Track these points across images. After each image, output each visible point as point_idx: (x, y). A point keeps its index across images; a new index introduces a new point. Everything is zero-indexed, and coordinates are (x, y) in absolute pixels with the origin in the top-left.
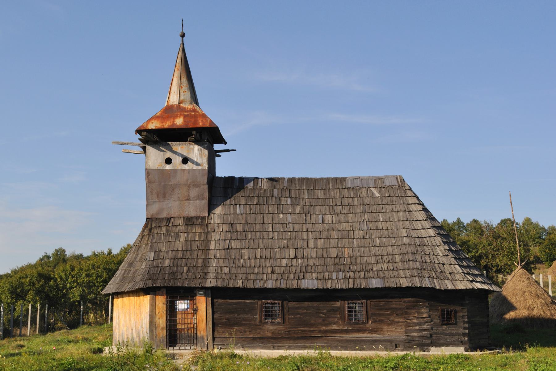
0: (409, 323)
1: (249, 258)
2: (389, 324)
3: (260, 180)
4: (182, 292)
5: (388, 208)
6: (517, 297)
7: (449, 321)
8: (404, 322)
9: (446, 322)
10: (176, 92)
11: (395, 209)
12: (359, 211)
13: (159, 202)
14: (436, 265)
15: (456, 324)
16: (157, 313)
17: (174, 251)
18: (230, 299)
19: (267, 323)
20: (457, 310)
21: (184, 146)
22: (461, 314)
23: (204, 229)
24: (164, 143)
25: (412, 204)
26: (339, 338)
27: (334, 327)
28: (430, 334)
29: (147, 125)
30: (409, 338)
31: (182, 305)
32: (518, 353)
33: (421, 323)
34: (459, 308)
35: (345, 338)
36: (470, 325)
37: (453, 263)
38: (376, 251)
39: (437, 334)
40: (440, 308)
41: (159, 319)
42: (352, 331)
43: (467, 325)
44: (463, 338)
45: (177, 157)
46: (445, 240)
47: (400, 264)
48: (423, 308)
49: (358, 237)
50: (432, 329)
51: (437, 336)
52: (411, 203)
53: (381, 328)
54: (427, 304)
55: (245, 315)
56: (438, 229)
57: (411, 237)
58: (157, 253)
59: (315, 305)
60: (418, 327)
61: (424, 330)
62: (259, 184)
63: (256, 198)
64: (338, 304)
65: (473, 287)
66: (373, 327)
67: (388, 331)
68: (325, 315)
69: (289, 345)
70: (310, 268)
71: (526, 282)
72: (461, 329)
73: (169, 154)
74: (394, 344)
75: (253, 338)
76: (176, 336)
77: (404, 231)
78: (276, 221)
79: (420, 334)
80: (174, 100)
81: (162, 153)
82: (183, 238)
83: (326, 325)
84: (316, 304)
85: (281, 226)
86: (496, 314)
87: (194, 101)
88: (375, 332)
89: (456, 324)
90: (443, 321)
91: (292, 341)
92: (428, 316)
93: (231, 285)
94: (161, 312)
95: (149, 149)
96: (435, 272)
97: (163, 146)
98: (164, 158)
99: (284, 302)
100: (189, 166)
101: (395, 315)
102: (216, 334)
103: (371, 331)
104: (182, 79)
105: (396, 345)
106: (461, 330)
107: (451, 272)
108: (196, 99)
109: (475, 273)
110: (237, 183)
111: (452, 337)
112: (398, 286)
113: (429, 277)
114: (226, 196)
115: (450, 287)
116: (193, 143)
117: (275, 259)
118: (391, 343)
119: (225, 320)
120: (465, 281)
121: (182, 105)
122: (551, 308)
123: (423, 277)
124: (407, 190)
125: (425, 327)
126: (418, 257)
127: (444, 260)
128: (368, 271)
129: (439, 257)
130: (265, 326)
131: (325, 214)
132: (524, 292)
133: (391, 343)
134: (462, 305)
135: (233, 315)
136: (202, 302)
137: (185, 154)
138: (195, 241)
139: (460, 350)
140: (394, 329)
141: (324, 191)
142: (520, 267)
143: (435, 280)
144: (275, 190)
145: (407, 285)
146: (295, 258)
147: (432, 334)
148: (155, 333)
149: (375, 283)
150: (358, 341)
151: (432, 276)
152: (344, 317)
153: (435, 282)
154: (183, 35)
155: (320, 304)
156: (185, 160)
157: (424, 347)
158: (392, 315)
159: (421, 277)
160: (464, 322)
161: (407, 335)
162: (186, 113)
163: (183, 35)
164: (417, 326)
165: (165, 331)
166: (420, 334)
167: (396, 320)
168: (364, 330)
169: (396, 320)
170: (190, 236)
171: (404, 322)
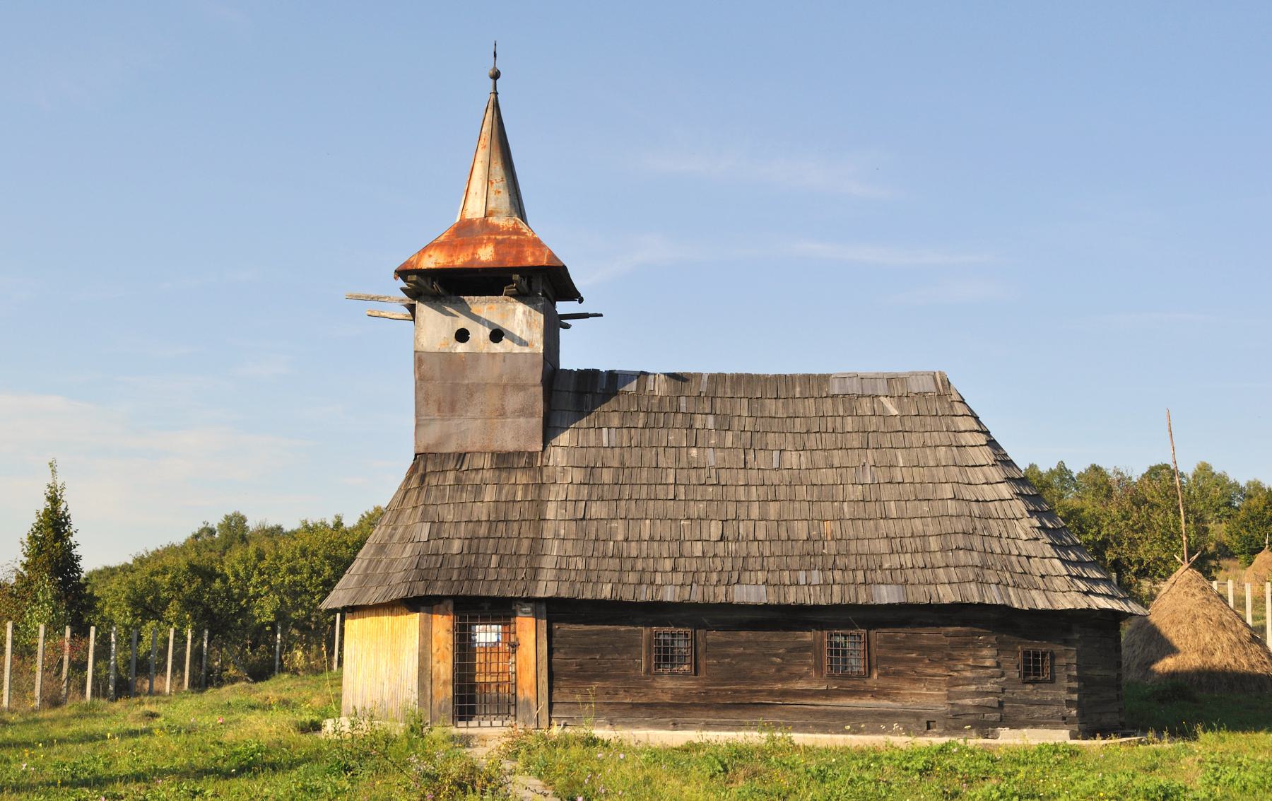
0: (956, 679)
1: (626, 540)
2: (914, 679)
3: (651, 377)
4: (486, 608)
5: (915, 439)
6: (1180, 627)
8: (946, 676)
11: (929, 441)
12: (856, 444)
13: (442, 420)
14: (1014, 559)
15: (1053, 681)
17: (471, 521)
18: (586, 624)
19: (663, 674)
20: (1055, 652)
21: (495, 306)
22: (1064, 661)
24: (454, 298)
25: (965, 431)
26: (809, 707)
27: (800, 685)
29: (419, 260)
30: (956, 709)
31: (486, 635)
33: (980, 678)
34: (1057, 648)
39: (1012, 702)
40: (1019, 647)
41: (438, 662)
43: (1075, 685)
44: (1066, 711)
45: (481, 326)
46: (1031, 508)
50: (1003, 690)
54: (993, 639)
55: (616, 656)
57: (963, 499)
59: (762, 639)
60: (973, 688)
61: (987, 693)
62: (650, 386)
63: (642, 414)
64: (809, 636)
65: (1089, 606)
68: (782, 659)
69: (707, 720)
70: (751, 560)
71: (1200, 596)
72: (1063, 691)
73: (463, 322)
74: (924, 721)
76: (472, 699)
78: (684, 463)
79: (978, 701)
80: (475, 209)
83: (783, 680)
84: (762, 636)
86: (1137, 661)
87: (516, 212)
88: (885, 695)
89: (1053, 681)
90: (1026, 675)
91: (712, 713)
92: (995, 664)
94: (442, 648)
96: (1010, 572)
97: (451, 304)
100: (505, 346)
101: (927, 661)
103: (875, 694)
104: (493, 165)
105: (928, 723)
106: (1063, 695)
107: (1044, 573)
109: (1095, 577)
111: (1044, 709)
113: (997, 584)
115: (1042, 604)
116: (513, 300)
119: (574, 667)
120: (1073, 593)
121: (491, 220)
122: (1249, 651)
123: (987, 583)
125: (989, 686)
126: (977, 542)
127: (1030, 548)
128: (872, 570)
129: (1019, 542)
130: (658, 680)
131: (784, 450)
132: (1195, 618)
133: (918, 720)
134: (1066, 642)
135: (593, 657)
136: (527, 629)
137: (497, 321)
139: (1061, 736)
141: (783, 403)
144: (683, 399)
146: (721, 540)
147: (1003, 702)
149: (887, 595)
150: (849, 713)
151: (1005, 582)
152: (822, 664)
153: (1011, 593)
154: (496, 76)
157: (985, 728)
158: (921, 660)
159: (981, 582)
160: (1070, 678)
162: (499, 237)
163: (496, 76)
164: (971, 684)
166: (978, 701)
167: (929, 671)
168: (864, 691)
169: (929, 671)
170: (504, 492)
171: (946, 676)
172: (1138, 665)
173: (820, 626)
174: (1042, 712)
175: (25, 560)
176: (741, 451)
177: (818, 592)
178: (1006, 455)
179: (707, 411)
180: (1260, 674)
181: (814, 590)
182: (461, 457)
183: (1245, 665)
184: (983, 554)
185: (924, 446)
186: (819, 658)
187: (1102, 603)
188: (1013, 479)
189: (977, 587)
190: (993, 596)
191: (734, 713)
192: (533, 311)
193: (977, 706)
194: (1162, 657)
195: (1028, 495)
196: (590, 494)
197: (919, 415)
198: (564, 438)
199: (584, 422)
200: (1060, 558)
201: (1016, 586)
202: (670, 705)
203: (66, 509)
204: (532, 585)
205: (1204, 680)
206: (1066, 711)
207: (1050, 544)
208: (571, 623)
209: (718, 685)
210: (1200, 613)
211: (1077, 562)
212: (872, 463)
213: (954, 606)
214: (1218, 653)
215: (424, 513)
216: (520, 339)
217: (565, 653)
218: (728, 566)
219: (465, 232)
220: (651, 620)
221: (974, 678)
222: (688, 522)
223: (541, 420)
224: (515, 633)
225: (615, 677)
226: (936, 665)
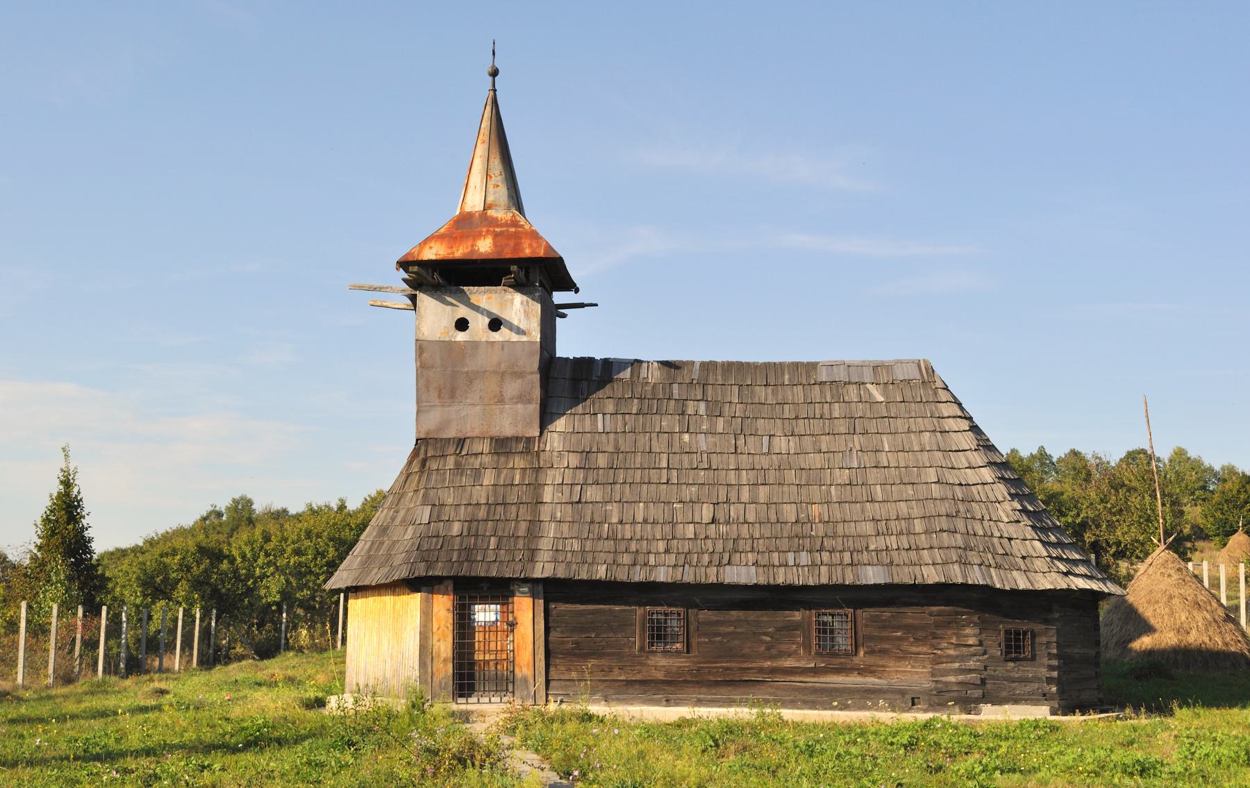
0: (940, 656)
1: (621, 522)
2: (899, 657)
3: (645, 365)
4: (485, 588)
5: (900, 425)
6: (1156, 606)
8: (930, 654)
9: (1013, 655)
11: (914, 427)
12: (843, 429)
13: (442, 406)
14: (996, 540)
15: (1033, 658)
16: (435, 629)
17: (470, 504)
21: (494, 296)
22: (1044, 639)
24: (453, 288)
25: (949, 417)
27: (789, 663)
29: (420, 252)
30: (940, 686)
31: (485, 614)
33: (963, 656)
34: (1038, 627)
35: (810, 684)
37: (1030, 537)
38: (874, 510)
39: (994, 680)
40: (1001, 626)
41: (439, 641)
43: (1055, 663)
44: (1046, 687)
46: (1013, 491)
48: (968, 625)
49: (839, 481)
50: (986, 668)
51: (994, 684)
53: (883, 666)
54: (975, 618)
55: (611, 635)
57: (947, 483)
60: (957, 665)
61: (970, 671)
62: (643, 373)
63: (636, 401)
64: (797, 616)
65: (1069, 586)
66: (867, 663)
67: (896, 671)
69: (699, 696)
70: (742, 542)
71: (1176, 577)
72: (1043, 669)
73: (463, 311)
74: (909, 697)
76: (471, 676)
78: (676, 448)
79: (961, 678)
80: (474, 202)
81: (449, 308)
82: (488, 478)
84: (752, 615)
86: (1115, 640)
87: (514, 204)
88: (871, 672)
90: (1007, 653)
91: (704, 690)
92: (977, 643)
93: (584, 576)
96: (992, 554)
97: (451, 294)
99: (690, 611)
100: (503, 335)
102: (553, 674)
103: (862, 672)
104: (491, 160)
105: (913, 699)
106: (1044, 672)
107: (1025, 554)
109: (1074, 558)
111: (1025, 686)
113: (980, 565)
115: (1023, 584)
119: (570, 646)
122: (1223, 630)
123: (970, 564)
124: (939, 390)
125: (971, 664)
126: (960, 525)
127: (1011, 530)
131: (774, 435)
132: (1171, 598)
133: (903, 697)
135: (588, 635)
136: (525, 608)
137: (495, 310)
139: (1041, 712)
143: (992, 570)
144: (675, 386)
145: (937, 580)
147: (985, 679)
148: (430, 670)
149: (873, 576)
150: (836, 690)
151: (987, 563)
152: (810, 642)
153: (993, 574)
154: (494, 73)
156: (495, 324)
158: (906, 639)
159: (964, 563)
160: (1050, 656)
162: (498, 230)
163: (494, 73)
164: (955, 662)
165: (450, 666)
166: (961, 678)
167: (914, 649)
169: (914, 649)
171: (930, 654)
172: (1116, 644)
173: (808, 606)
175: (39, 541)
177: (807, 573)
178: (988, 440)
180: (1234, 652)
184: (966, 536)
187: (1081, 584)
188: (995, 464)
190: (976, 577)
191: (724, 690)
192: (530, 300)
194: (1139, 636)
195: (1010, 479)
197: (904, 402)
198: (560, 424)
199: (579, 409)
203: (79, 492)
204: (529, 566)
205: (1180, 658)
206: (1046, 687)
207: (1031, 526)
208: (567, 603)
209: (709, 662)
211: (1057, 543)
212: (858, 448)
213: (938, 587)
214: (1194, 632)
216: (518, 328)
217: (562, 632)
218: (719, 547)
219: (465, 225)
220: (644, 600)
221: (957, 656)
224: (513, 612)
225: (610, 654)
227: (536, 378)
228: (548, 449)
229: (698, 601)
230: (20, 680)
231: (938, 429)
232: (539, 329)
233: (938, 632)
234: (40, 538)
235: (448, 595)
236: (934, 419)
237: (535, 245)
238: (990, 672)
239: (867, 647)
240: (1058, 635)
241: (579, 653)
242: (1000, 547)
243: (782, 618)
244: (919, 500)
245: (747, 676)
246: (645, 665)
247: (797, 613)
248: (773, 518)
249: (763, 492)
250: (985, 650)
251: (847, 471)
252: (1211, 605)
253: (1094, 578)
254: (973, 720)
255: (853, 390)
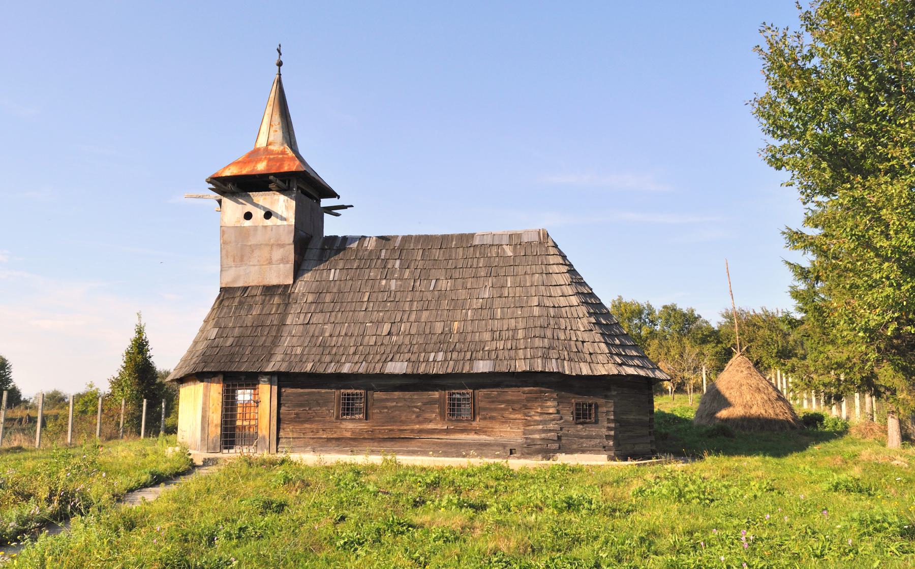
0: (529, 421)
1: (331, 336)
2: (503, 422)
3: (368, 239)
4: (243, 379)
5: (521, 270)
6: (732, 391)
7: (587, 418)
8: (523, 419)
9: (581, 420)
10: (265, 132)
11: (529, 271)
12: (483, 274)
13: (236, 267)
14: (573, 343)
15: (596, 422)
16: (211, 406)
17: (242, 327)
18: (302, 388)
19: (346, 419)
20: (598, 403)
21: (267, 197)
22: (605, 409)
23: (284, 300)
24: (244, 194)
25: (553, 264)
26: (436, 440)
27: (431, 426)
28: (558, 436)
29: (223, 172)
30: (529, 441)
31: (243, 395)
32: (432, 478)
33: (545, 421)
34: (601, 401)
36: (618, 424)
37: (597, 341)
38: (494, 325)
39: (568, 437)
40: (573, 400)
41: (213, 413)
42: (454, 431)
43: (613, 425)
44: (605, 442)
45: (258, 210)
46: (592, 311)
47: (522, 341)
48: (549, 400)
49: (475, 307)
50: (561, 429)
51: (568, 439)
52: (552, 263)
53: (492, 428)
54: (555, 395)
55: (319, 408)
56: (586, 297)
57: (544, 306)
58: (221, 329)
59: (407, 397)
60: (540, 427)
61: (550, 431)
62: (365, 244)
63: (357, 260)
64: (436, 395)
65: (619, 372)
66: (481, 426)
67: (500, 431)
68: (420, 409)
69: (372, 448)
70: (403, 346)
71: (745, 372)
72: (603, 429)
73: (249, 208)
74: (508, 449)
75: (327, 438)
76: (233, 436)
77: (536, 299)
78: (376, 289)
79: (543, 435)
80: (262, 143)
81: (240, 206)
82: (256, 311)
83: (420, 423)
84: (408, 395)
85: (380, 295)
86: (706, 412)
87: (287, 142)
88: (483, 432)
89: (596, 422)
90: (577, 418)
91: (376, 444)
92: (555, 412)
93: (297, 370)
94: (215, 404)
95: (225, 200)
96: (568, 351)
97: (242, 197)
98: (243, 212)
99: (368, 392)
100: (273, 221)
101: (511, 410)
102: (282, 434)
103: (477, 432)
104: (274, 115)
105: (511, 450)
106: (604, 432)
107: (591, 352)
108: (292, 141)
109: (632, 354)
110: (338, 244)
111: (590, 441)
112: (512, 370)
113: (557, 359)
114: (322, 258)
115: (585, 371)
116: (278, 193)
117: (363, 336)
118: (504, 448)
119: (293, 416)
120: (610, 365)
121: (270, 147)
122: (775, 406)
123: (549, 358)
124: (550, 248)
125: (551, 426)
126: (549, 333)
127: (586, 336)
128: (477, 350)
129: (578, 333)
130: (344, 423)
131: (439, 279)
132: (741, 385)
133: (504, 448)
134: (606, 397)
136: (266, 392)
137: (269, 207)
138: (270, 314)
139: (600, 460)
140: (509, 429)
141: (444, 252)
142: (739, 354)
143: (566, 362)
144: (384, 251)
145: (524, 369)
146: (388, 334)
147: (561, 436)
148: (207, 432)
149: (483, 367)
150: (460, 444)
151: (563, 358)
152: (444, 412)
153: (566, 365)
154: (280, 64)
155: (415, 395)
156: (268, 215)
157: (547, 453)
158: (507, 409)
159: (546, 358)
160: (609, 421)
161: (526, 436)
162: (272, 157)
163: (280, 64)
164: (539, 425)
165: (219, 429)
166: (543, 435)
167: (512, 416)
168: (470, 430)
169: (512, 416)
170: (265, 309)
171: (523, 419)
172: (707, 415)
173: (443, 388)
174: (589, 443)
175: (124, 365)
176: (413, 281)
177: (439, 366)
178: (582, 279)
179: (396, 258)
180: (782, 420)
181: (438, 365)
182: (245, 289)
183: (772, 414)
184: (551, 341)
185: (525, 274)
186: (442, 408)
187: (631, 371)
188: (583, 293)
189: (542, 361)
190: (553, 366)
191: (389, 444)
192: (289, 199)
193: (543, 439)
194: (720, 410)
195: (592, 304)
196: (315, 309)
197: (525, 255)
198: (308, 276)
199: (322, 267)
200: (606, 343)
201: (570, 360)
202: (351, 439)
203: (146, 337)
204: (265, 364)
205: (745, 423)
206: (605, 442)
207: (601, 333)
208: (293, 388)
209: (379, 426)
210: (745, 383)
211: (620, 345)
212: (491, 285)
213: (524, 373)
214: (755, 407)
215: (217, 322)
216: (281, 216)
217: (288, 407)
218: (388, 351)
219: (254, 155)
220: (340, 386)
221: (541, 421)
222: (371, 324)
223: (293, 265)
224: (258, 394)
226: (517, 412)
227: (291, 249)
228: (296, 291)
229: (373, 385)
230: (69, 440)
231: (544, 272)
232: (293, 216)
233: (529, 404)
234: (125, 362)
235: (220, 383)
236: (543, 266)
237: (291, 164)
238: (564, 431)
239: (482, 415)
240: (615, 406)
241: (298, 420)
242: (575, 347)
243: (427, 397)
244: (524, 317)
245: (404, 435)
246: (339, 428)
247: (436, 393)
248: (427, 331)
249: (425, 315)
250: (561, 417)
251: (481, 300)
252: (768, 390)
253: (645, 368)
254: (414, 467)
255: (494, 250)
